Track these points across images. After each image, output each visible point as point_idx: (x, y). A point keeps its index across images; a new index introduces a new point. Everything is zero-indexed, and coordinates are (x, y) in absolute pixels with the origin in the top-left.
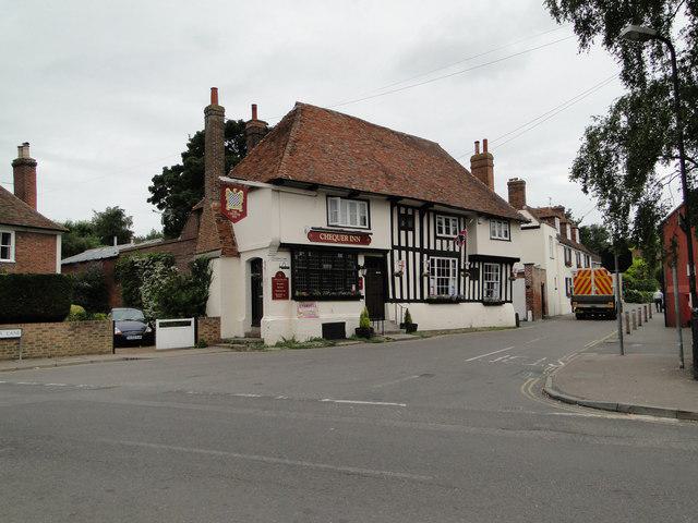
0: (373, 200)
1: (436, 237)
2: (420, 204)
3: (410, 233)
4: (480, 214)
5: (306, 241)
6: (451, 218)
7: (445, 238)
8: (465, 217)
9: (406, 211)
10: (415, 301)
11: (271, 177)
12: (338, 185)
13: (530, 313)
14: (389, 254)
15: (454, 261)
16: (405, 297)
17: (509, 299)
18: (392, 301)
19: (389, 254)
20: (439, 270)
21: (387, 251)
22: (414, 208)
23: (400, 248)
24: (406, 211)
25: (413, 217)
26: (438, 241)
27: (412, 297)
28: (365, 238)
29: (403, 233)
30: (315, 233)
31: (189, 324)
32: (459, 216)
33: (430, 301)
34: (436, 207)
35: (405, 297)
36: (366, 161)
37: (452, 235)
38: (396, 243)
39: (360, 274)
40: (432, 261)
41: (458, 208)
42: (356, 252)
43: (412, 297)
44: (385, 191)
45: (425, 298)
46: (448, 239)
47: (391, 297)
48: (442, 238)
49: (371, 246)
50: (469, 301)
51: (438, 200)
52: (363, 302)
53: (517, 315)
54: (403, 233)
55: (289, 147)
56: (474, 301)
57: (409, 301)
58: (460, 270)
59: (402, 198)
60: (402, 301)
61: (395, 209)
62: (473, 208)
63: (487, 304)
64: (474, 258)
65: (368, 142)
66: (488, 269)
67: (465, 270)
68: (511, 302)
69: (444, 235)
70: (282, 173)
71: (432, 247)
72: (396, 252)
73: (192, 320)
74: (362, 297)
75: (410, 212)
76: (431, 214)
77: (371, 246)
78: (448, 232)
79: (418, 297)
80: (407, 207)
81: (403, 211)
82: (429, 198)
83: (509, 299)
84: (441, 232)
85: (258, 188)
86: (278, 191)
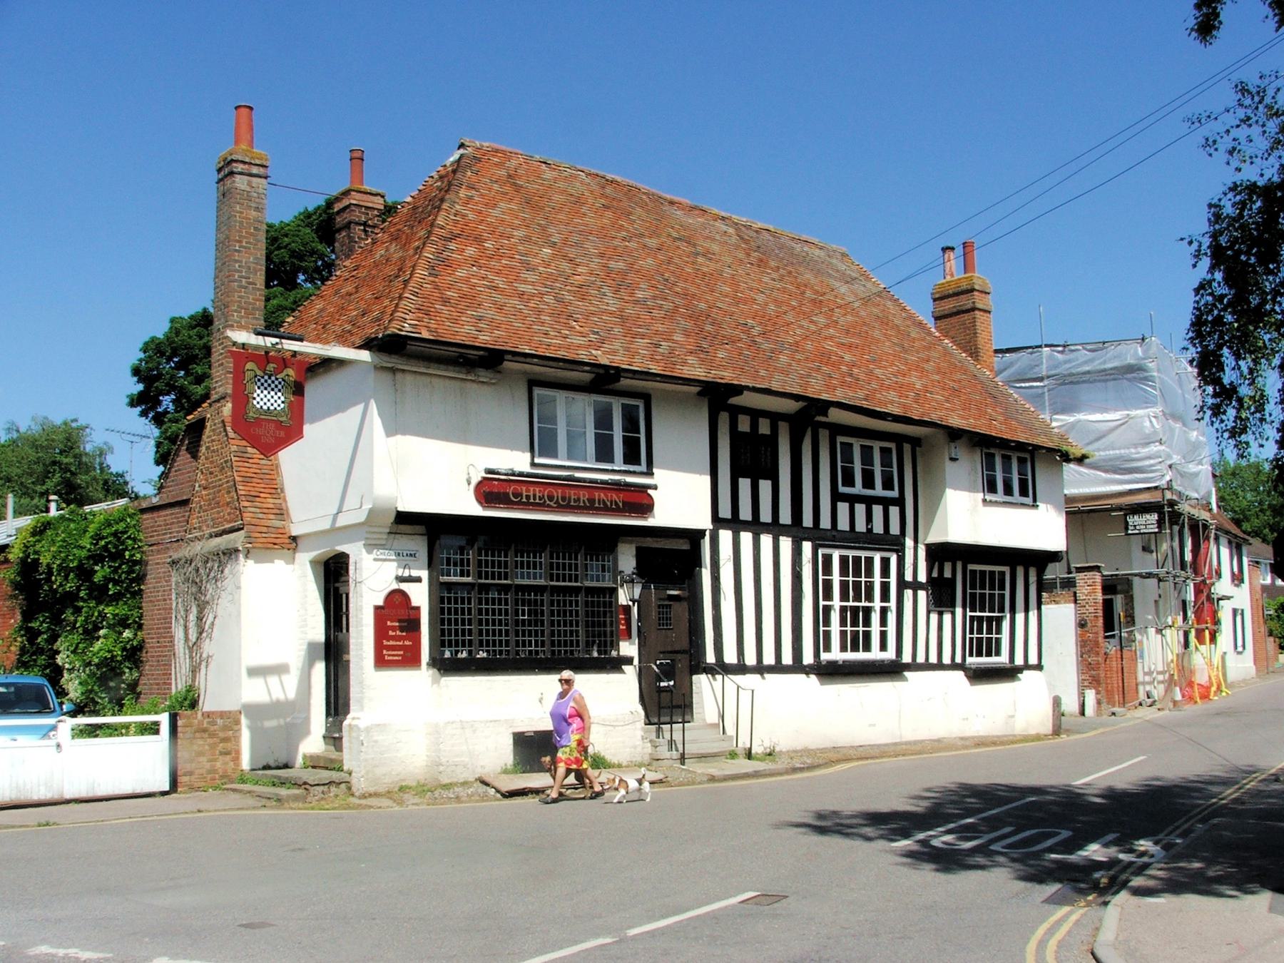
0: (670, 398)
1: (836, 497)
2: (790, 406)
3: (765, 486)
4: (954, 434)
5: (473, 508)
6: (877, 446)
7: (878, 500)
8: (916, 442)
9: (754, 425)
10: (778, 668)
11: (371, 331)
12: (561, 354)
13: (1091, 696)
14: (707, 538)
15: (885, 563)
16: (750, 660)
17: (1033, 660)
18: (710, 670)
19: (707, 538)
20: (844, 586)
21: (701, 533)
22: (775, 417)
23: (735, 523)
24: (754, 425)
25: (772, 441)
26: (843, 508)
27: (769, 659)
28: (640, 501)
29: (745, 484)
30: (490, 489)
31: (153, 729)
32: (899, 439)
33: (830, 672)
34: (835, 415)
35: (750, 660)
36: (224, 445)
37: (879, 491)
38: (725, 512)
39: (623, 598)
40: (828, 560)
41: (21, 826)
42: (606, 540)
43: (769, 659)
44: (695, 370)
45: (808, 659)
46: (869, 502)
47: (710, 658)
48: (852, 500)
49: (650, 522)
50: (927, 666)
51: (839, 395)
52: (631, 672)
53: (1057, 702)
54: (745, 484)
55: (428, 253)
56: (940, 666)
57: (760, 669)
58: (902, 584)
59: (738, 390)
60: (741, 669)
61: (724, 419)
62: (934, 417)
63: (980, 676)
64: (940, 553)
65: (652, 242)
66: (974, 580)
67: (916, 586)
68: (1039, 667)
69: (858, 489)
70: (406, 325)
71: (825, 523)
72: (725, 536)
73: (164, 719)
74: (629, 661)
75: (764, 428)
76: (824, 436)
77: (659, 518)
78: (868, 482)
79: (787, 659)
80: (755, 414)
81: (744, 425)
82: (817, 389)
83: (1033, 660)
84: (849, 481)
85: (341, 363)
86: (393, 371)
